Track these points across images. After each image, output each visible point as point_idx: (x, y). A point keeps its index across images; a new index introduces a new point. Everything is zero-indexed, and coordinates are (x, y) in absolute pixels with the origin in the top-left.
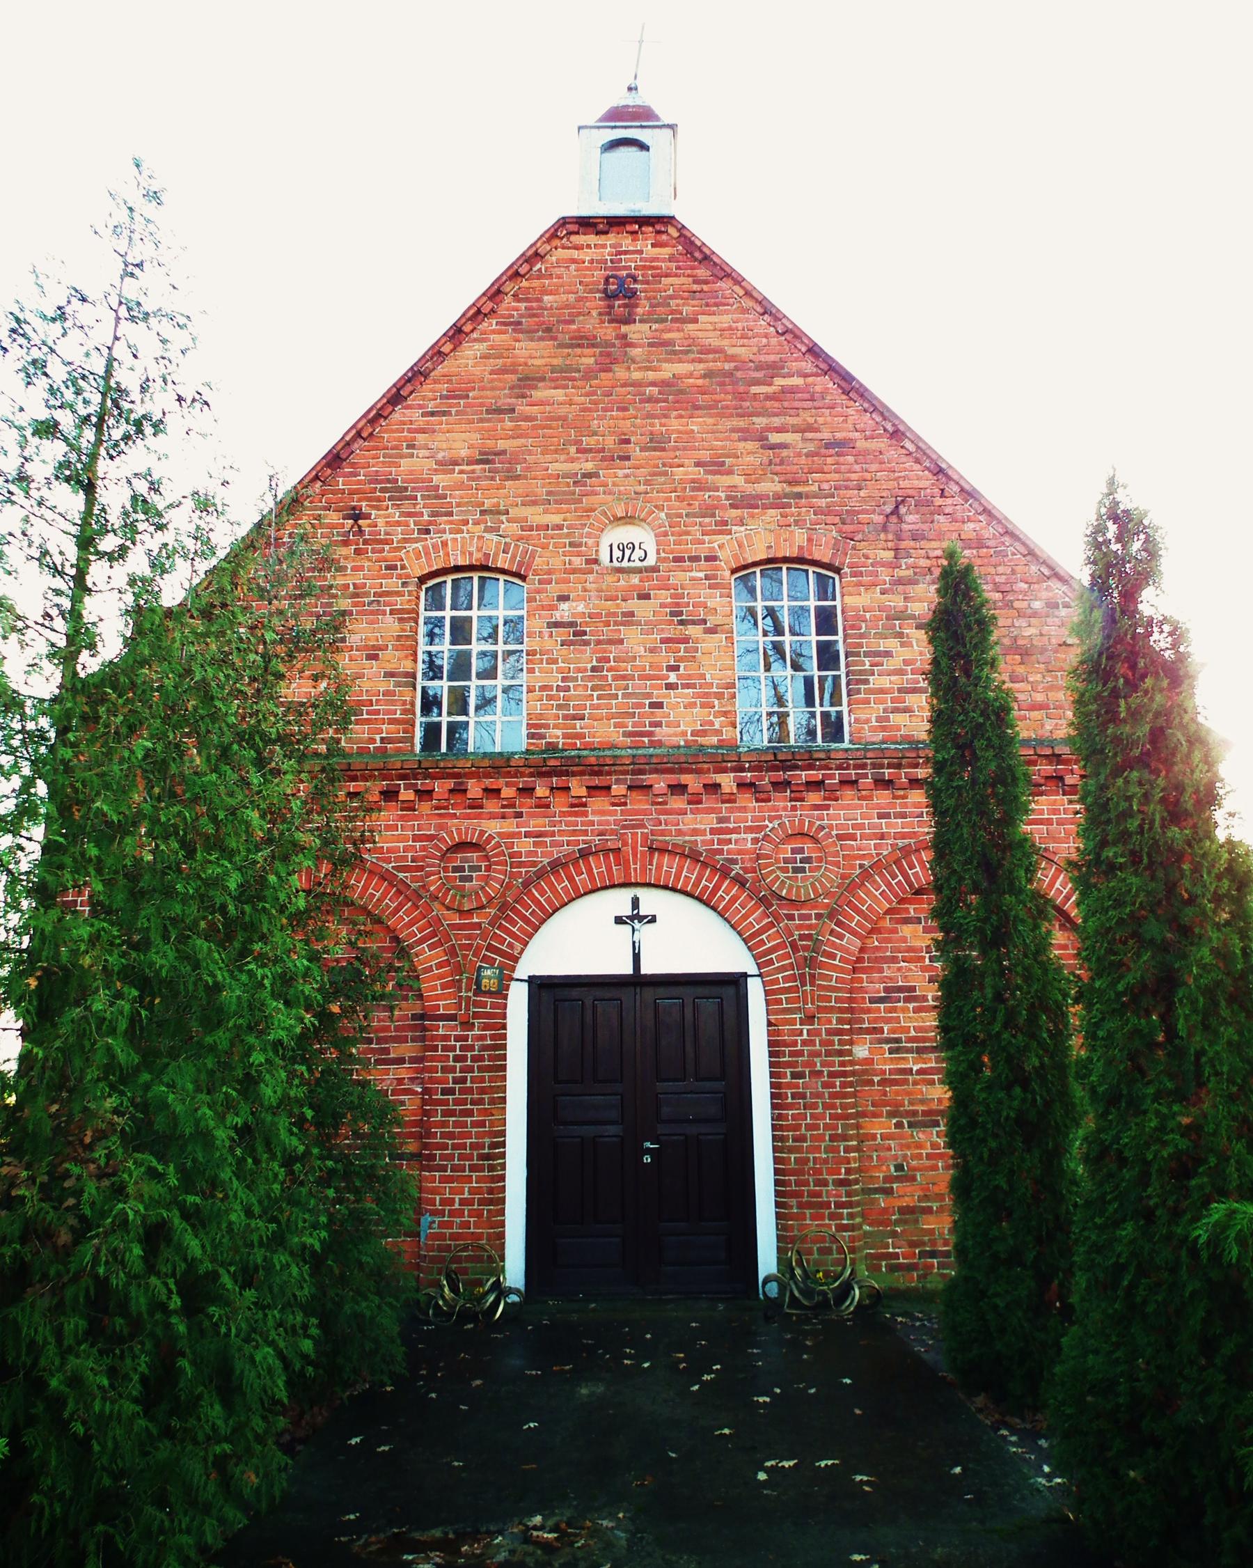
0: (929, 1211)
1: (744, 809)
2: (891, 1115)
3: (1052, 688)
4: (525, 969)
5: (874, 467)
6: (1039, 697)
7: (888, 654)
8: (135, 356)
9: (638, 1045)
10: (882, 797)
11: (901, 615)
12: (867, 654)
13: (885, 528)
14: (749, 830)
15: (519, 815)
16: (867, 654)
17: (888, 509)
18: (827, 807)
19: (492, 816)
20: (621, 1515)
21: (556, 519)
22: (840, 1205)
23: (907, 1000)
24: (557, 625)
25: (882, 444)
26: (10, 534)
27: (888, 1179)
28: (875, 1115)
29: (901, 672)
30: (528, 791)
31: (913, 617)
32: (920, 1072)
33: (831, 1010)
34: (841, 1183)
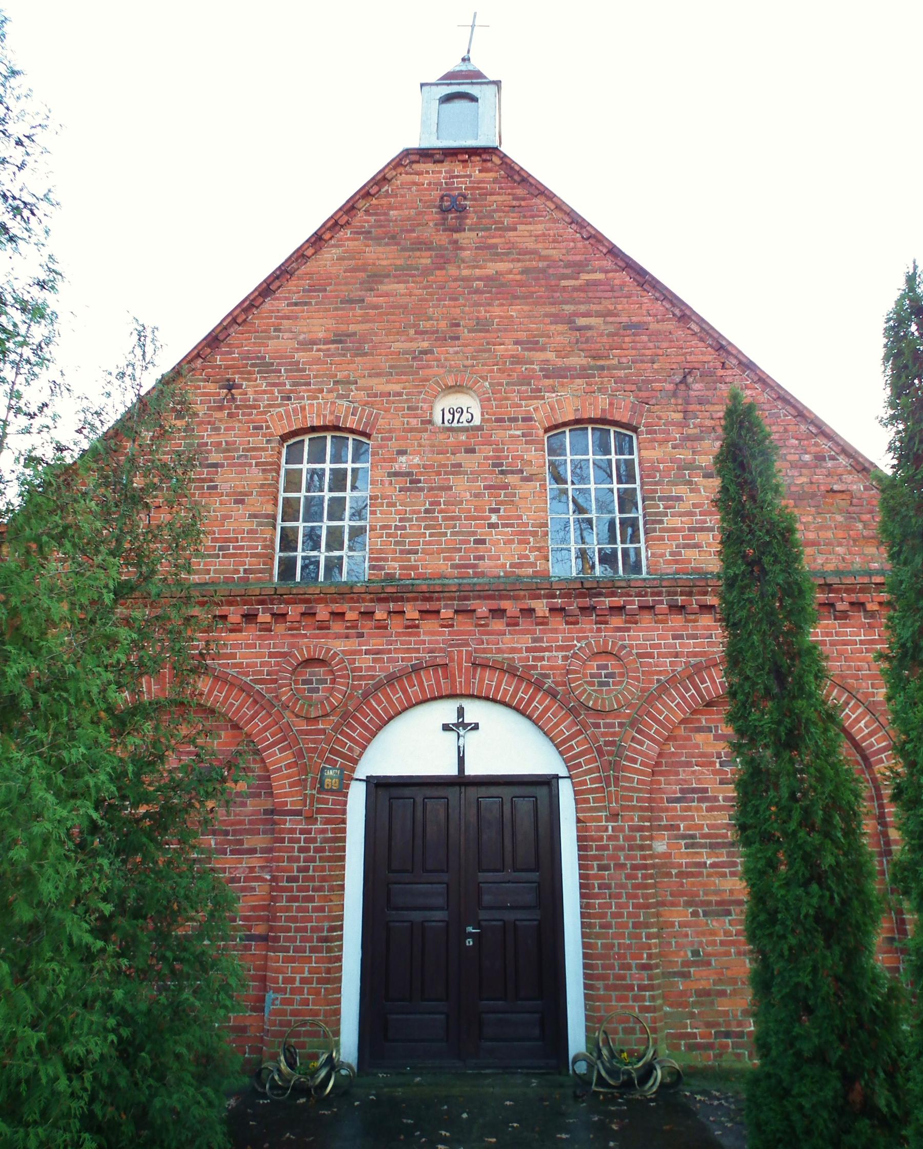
0: (722, 993)
1: (556, 631)
2: (688, 904)
7: (679, 499)
10: (676, 621)
11: (691, 466)
12: (660, 499)
13: (675, 395)
14: (560, 648)
15: (361, 635)
16: (660, 499)
17: (678, 379)
23: (700, 800)
24: (396, 474)
25: (670, 326)
28: (673, 904)
29: (691, 514)
31: (700, 468)
32: (713, 865)
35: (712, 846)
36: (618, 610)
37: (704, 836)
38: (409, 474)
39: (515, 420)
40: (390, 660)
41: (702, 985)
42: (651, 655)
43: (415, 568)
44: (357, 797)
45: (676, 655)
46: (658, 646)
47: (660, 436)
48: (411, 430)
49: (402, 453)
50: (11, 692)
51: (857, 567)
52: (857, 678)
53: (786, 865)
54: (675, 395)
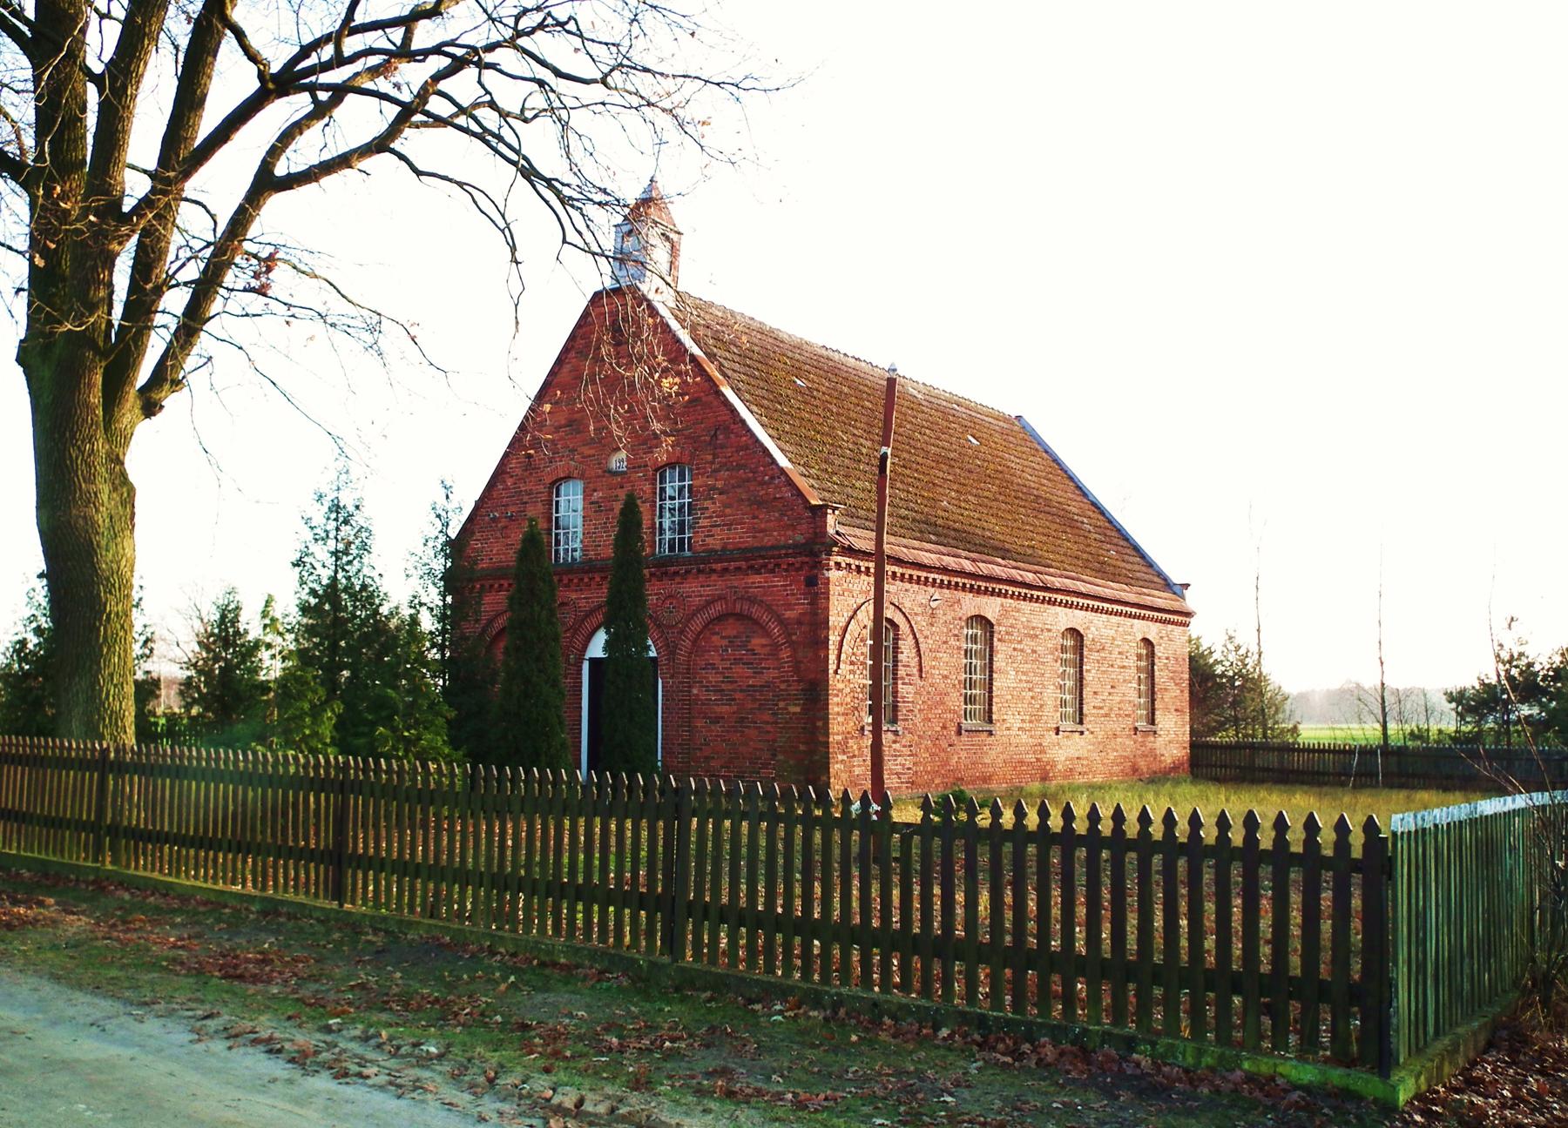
0: (713, 758)
1: (654, 585)
2: (704, 718)
3: (769, 521)
4: (587, 657)
5: (708, 411)
6: (763, 526)
7: (707, 508)
8: (447, 497)
9: (231, 808)
10: (702, 578)
11: (713, 488)
12: (700, 509)
13: (710, 444)
14: (656, 594)
15: (581, 590)
16: (700, 509)
17: (712, 433)
18: (682, 583)
19: (573, 591)
20: (854, 1038)
21: (592, 452)
22: (679, 753)
23: (713, 669)
24: (592, 503)
25: (711, 398)
26: (408, 84)
27: (701, 744)
28: (698, 718)
29: (711, 517)
30: (582, 579)
31: (718, 489)
32: (715, 700)
33: (679, 673)
34: (679, 744)
35: (714, 691)
36: (676, 573)
37: (713, 686)
38: (597, 502)
39: (639, 467)
40: (593, 602)
41: (706, 754)
42: (691, 597)
43: (599, 554)
44: (586, 666)
45: (701, 596)
46: (694, 592)
47: (701, 471)
48: (599, 477)
49: (595, 491)
50: (148, 672)
51: (782, 543)
52: (777, 605)
53: (310, 716)
54: (710, 444)
